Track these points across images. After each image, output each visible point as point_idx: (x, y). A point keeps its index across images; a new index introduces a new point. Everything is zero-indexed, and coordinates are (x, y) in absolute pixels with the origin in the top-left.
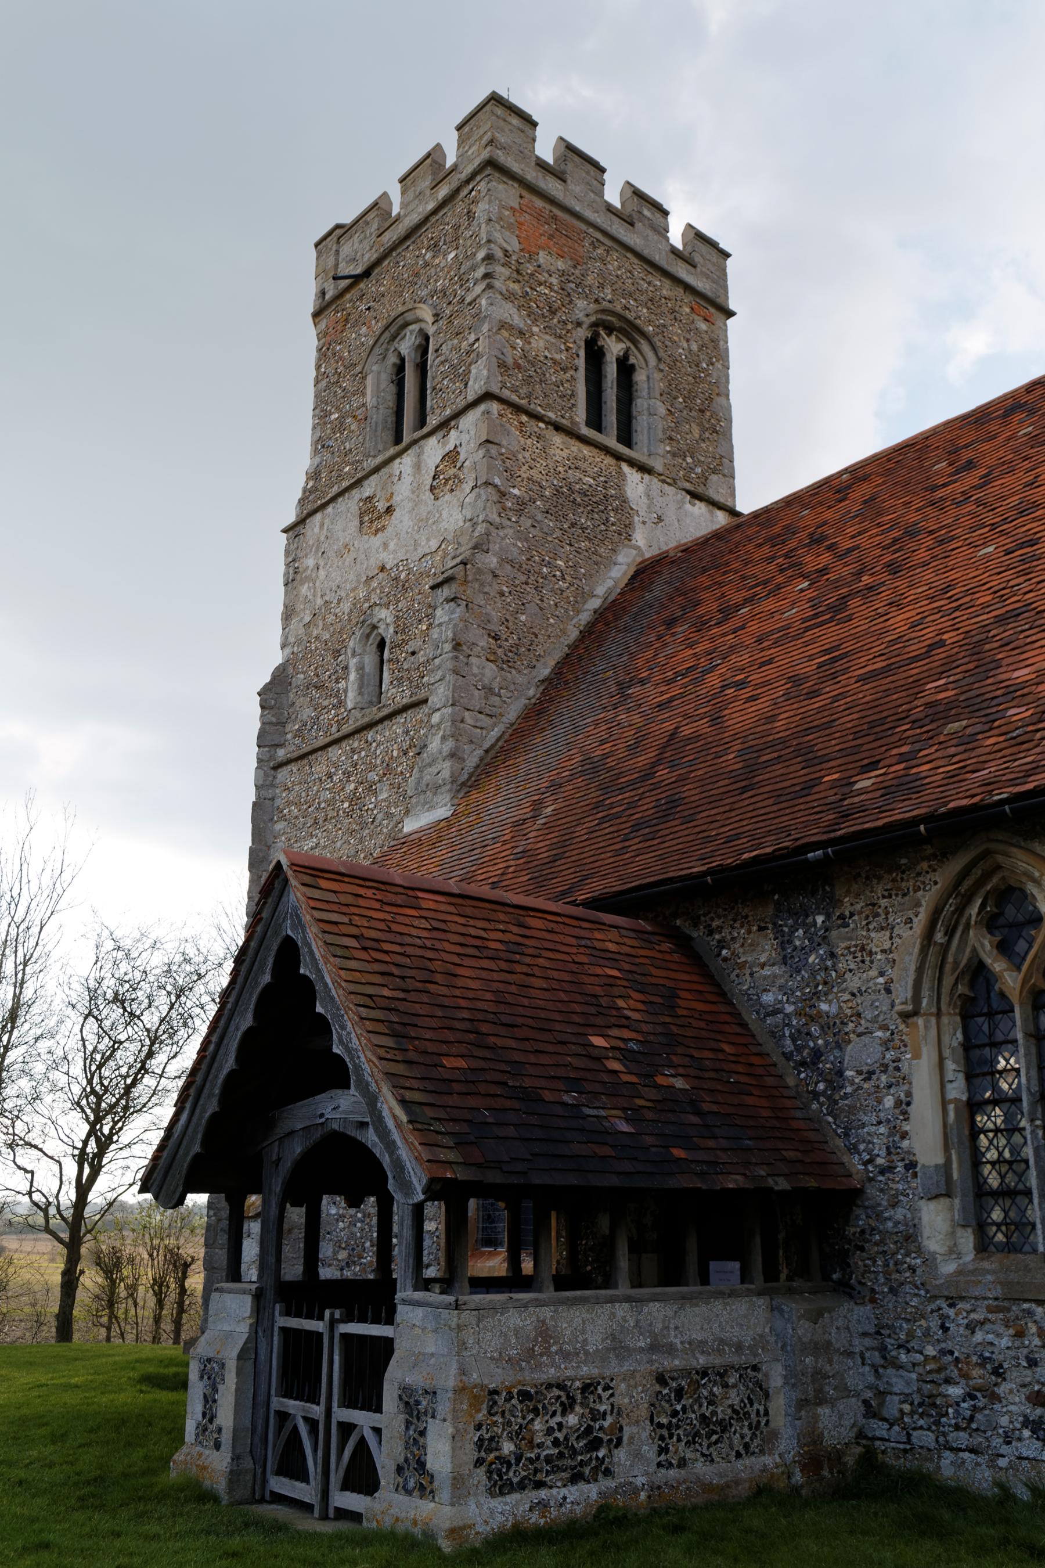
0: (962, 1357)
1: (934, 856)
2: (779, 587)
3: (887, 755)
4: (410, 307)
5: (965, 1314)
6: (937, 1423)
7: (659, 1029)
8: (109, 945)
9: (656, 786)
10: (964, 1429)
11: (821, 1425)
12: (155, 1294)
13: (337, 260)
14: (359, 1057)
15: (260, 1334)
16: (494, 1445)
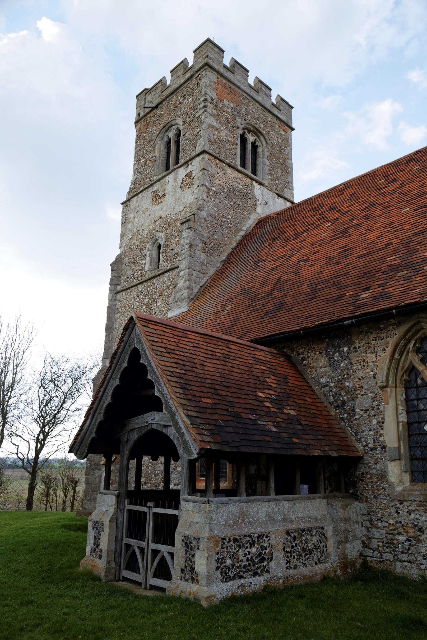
0: (405, 524)
1: (395, 324)
2: (318, 225)
3: (373, 284)
4: (174, 119)
5: (406, 507)
6: (394, 551)
7: (283, 391)
8: (50, 360)
9: (273, 298)
10: (406, 553)
11: (347, 551)
12: (64, 492)
13: (145, 102)
14: (167, 397)
15: (119, 512)
16: (223, 561)
